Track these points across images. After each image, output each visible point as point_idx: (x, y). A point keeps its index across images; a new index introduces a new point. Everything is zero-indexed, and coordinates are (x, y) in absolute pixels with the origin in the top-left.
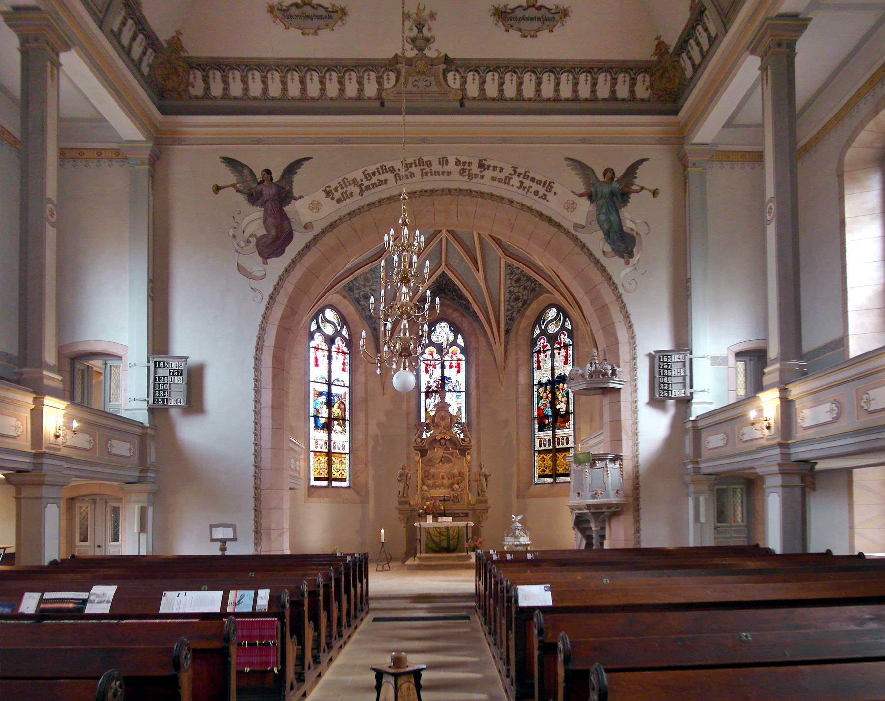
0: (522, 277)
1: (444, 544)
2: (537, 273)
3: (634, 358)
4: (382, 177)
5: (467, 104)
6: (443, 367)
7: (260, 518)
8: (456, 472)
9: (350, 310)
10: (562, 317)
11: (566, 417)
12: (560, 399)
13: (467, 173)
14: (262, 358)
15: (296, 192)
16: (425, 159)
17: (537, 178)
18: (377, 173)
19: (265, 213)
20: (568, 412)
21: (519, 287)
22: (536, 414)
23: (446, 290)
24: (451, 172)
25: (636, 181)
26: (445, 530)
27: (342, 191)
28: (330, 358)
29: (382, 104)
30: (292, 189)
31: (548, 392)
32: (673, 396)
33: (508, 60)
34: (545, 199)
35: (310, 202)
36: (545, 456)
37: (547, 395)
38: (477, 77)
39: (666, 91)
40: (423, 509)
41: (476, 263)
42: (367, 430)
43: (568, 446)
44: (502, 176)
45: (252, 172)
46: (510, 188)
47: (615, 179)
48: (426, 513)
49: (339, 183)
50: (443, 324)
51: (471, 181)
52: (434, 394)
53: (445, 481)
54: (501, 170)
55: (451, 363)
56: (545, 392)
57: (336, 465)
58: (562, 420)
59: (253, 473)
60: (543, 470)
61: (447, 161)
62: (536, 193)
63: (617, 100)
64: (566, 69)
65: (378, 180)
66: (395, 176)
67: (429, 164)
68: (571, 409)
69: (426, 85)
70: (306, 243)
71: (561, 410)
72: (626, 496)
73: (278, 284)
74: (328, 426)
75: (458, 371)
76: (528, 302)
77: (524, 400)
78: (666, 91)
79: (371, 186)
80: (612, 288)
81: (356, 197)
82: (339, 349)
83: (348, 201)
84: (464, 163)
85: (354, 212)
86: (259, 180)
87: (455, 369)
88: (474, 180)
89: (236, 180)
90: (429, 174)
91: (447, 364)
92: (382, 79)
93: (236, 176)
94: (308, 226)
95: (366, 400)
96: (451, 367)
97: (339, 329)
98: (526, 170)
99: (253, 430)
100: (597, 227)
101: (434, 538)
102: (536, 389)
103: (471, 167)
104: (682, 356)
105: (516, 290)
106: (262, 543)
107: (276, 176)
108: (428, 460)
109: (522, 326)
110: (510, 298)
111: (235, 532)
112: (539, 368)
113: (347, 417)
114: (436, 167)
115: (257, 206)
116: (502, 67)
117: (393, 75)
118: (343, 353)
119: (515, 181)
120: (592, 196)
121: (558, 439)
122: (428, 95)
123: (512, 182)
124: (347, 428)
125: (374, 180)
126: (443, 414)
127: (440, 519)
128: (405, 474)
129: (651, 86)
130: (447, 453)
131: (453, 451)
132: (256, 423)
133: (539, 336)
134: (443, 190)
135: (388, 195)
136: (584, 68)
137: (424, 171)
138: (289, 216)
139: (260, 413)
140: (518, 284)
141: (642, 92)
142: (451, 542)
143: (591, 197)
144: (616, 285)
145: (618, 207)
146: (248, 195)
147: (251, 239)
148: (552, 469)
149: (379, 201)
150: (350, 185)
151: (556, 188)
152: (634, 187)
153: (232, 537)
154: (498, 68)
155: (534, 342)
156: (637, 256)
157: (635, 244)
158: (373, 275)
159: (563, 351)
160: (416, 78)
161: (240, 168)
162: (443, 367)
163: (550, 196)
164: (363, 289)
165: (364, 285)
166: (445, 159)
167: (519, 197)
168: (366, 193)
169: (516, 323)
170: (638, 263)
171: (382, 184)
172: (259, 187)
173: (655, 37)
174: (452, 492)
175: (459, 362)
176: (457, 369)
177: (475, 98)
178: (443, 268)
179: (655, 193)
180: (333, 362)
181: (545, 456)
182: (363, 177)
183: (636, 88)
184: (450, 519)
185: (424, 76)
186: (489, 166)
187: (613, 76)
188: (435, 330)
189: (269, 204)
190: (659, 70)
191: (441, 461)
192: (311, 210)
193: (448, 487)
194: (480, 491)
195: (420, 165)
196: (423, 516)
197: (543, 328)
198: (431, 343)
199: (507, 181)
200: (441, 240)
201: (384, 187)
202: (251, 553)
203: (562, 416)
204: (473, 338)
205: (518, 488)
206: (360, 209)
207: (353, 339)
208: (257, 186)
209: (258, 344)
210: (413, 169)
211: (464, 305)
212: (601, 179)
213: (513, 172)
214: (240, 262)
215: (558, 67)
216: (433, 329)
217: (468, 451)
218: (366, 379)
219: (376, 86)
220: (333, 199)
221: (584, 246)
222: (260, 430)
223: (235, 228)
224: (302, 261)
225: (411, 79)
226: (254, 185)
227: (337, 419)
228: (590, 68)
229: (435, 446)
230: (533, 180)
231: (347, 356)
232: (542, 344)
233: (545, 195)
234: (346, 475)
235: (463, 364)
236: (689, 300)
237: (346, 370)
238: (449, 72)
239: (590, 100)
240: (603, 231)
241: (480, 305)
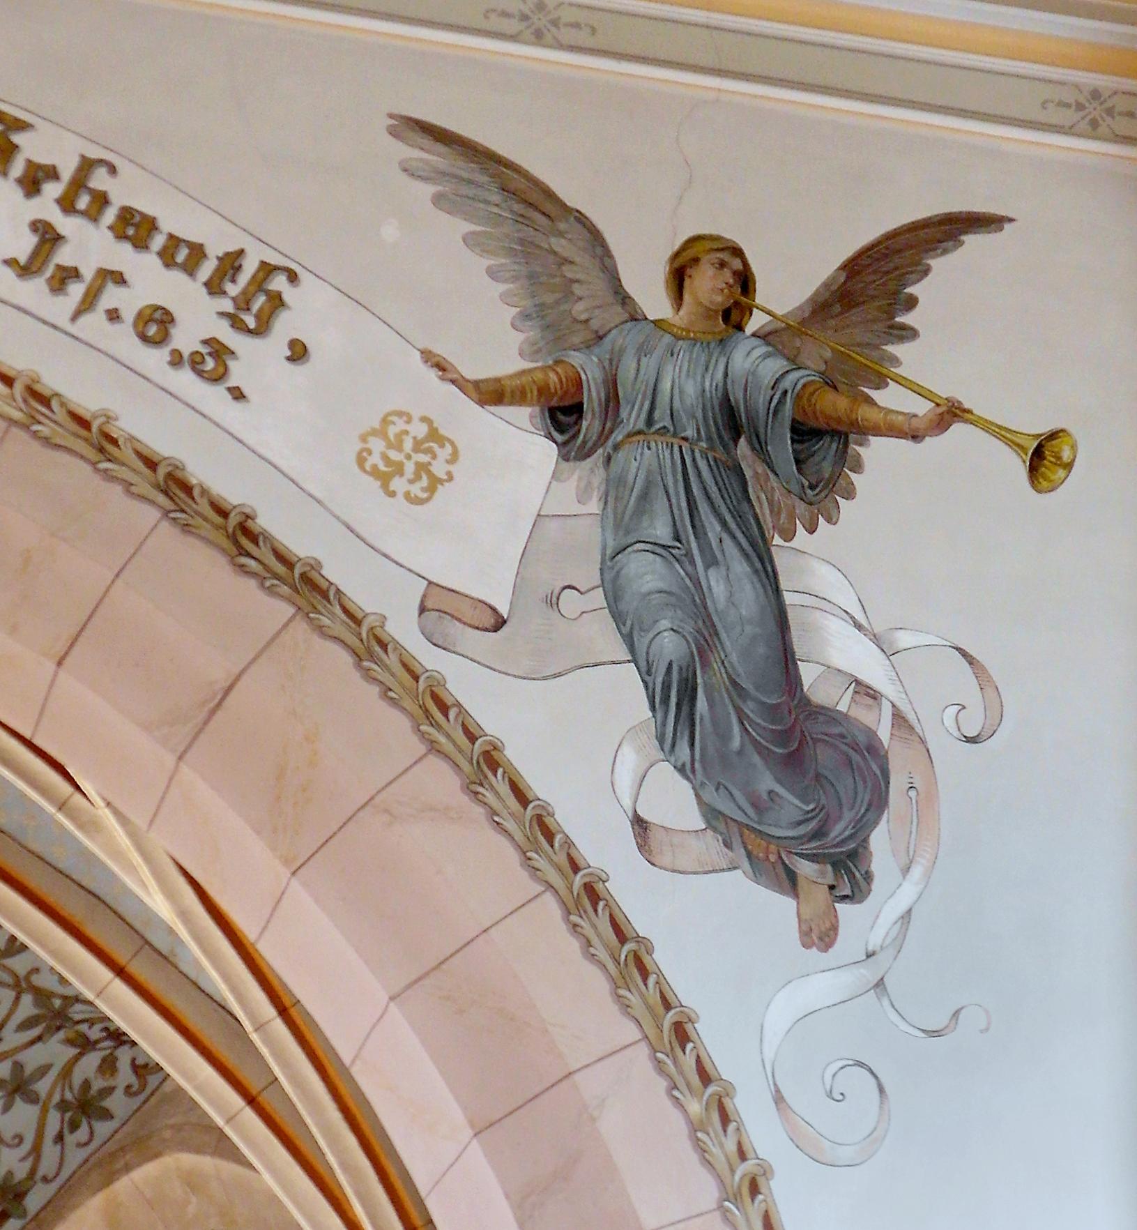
2: (120, 972)
17: (169, 223)
34: (217, 377)
47: (756, 322)
80: (695, 1108)
98: (94, 153)
120: (577, 410)
152: (890, 398)
157: (879, 802)
221: (492, 759)
240: (646, 673)
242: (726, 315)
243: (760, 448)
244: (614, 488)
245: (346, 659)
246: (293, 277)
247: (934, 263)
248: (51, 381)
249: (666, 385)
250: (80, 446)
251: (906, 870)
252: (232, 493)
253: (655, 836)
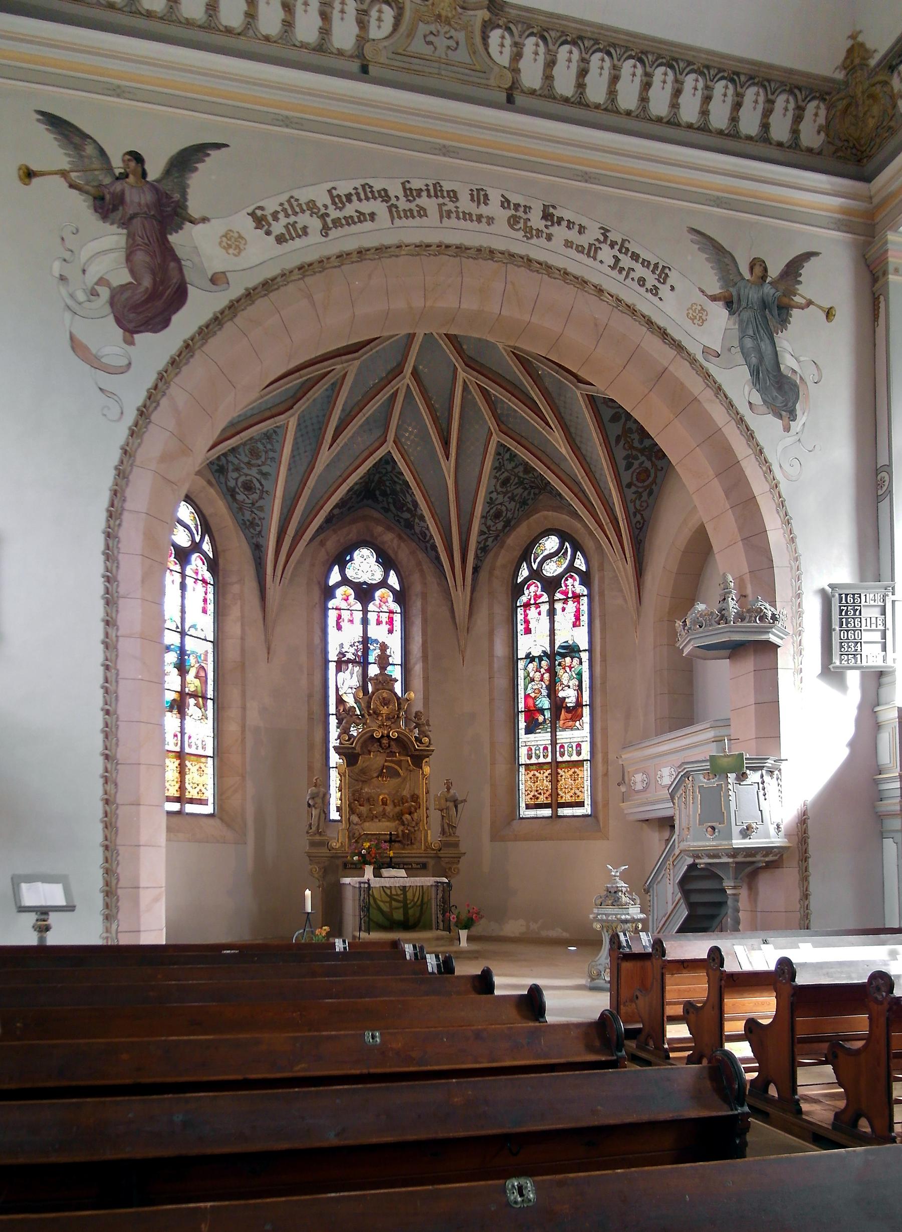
0: (513, 477)
1: (398, 915)
2: (548, 468)
3: (799, 596)
4: (367, 207)
5: (519, 99)
6: (365, 622)
7: (115, 864)
8: (406, 793)
9: (219, 508)
10: (569, 550)
11: (575, 712)
12: (565, 683)
13: (521, 225)
14: (122, 533)
15: (194, 207)
16: (446, 186)
17: (642, 256)
18: (354, 198)
19: (131, 241)
20: (579, 704)
21: (505, 494)
22: (521, 706)
23: (377, 493)
24: (493, 218)
25: (800, 288)
26: (399, 892)
27: (287, 220)
28: (183, 587)
29: (365, 69)
30: (186, 200)
31: (543, 671)
32: (864, 664)
33: (601, 27)
34: (656, 294)
35: (223, 232)
36: (537, 774)
37: (542, 675)
38: (542, 49)
39: (847, 141)
40: (359, 854)
41: (446, 443)
42: (244, 718)
43: (580, 758)
44: (584, 240)
45: (102, 152)
46: (596, 264)
47: (769, 280)
48: (365, 861)
49: (281, 204)
50: (365, 552)
51: (530, 241)
52: (350, 665)
53: (388, 809)
54: (582, 230)
55: (379, 617)
56: (538, 670)
57: (192, 776)
58: (570, 715)
59: (100, 770)
60: (534, 796)
61: (486, 196)
62: (642, 281)
63: (771, 144)
64: (695, 67)
65: (357, 211)
66: (390, 208)
67: (453, 196)
68: (586, 698)
69: (449, 47)
70: (215, 314)
71: (567, 700)
72: (788, 835)
73: (156, 387)
74: (179, 706)
75: (391, 631)
76: (512, 523)
77: (502, 682)
78: (847, 141)
79: (343, 222)
80: (764, 468)
81: (314, 237)
82: (197, 573)
83: (298, 243)
84: (517, 206)
85: (310, 265)
86: (117, 172)
87: (385, 627)
88: (534, 241)
89: (69, 163)
90: (454, 215)
91: (372, 617)
92: (367, 18)
93: (69, 155)
94: (218, 279)
95: (243, 666)
96: (379, 623)
97: (198, 539)
98: (625, 238)
99: (101, 680)
100: (740, 359)
101: (381, 904)
102: (521, 664)
103: (529, 216)
104: (878, 597)
105: (500, 499)
106: (120, 916)
107: (155, 170)
108: (361, 770)
109: (500, 561)
110: (489, 512)
111: (16, 893)
112: (528, 631)
113: (210, 694)
114: (465, 204)
115: (112, 224)
116: (590, 39)
117: (389, 13)
118: (204, 581)
119: (606, 254)
120: (732, 302)
121: (562, 747)
122: (450, 68)
123: (601, 255)
124: (210, 713)
125: (350, 210)
126: (385, 695)
127: (385, 872)
128: (321, 795)
129: (826, 128)
130: (392, 761)
131: (403, 758)
132: (107, 668)
133: (526, 580)
134: (479, 250)
135: (376, 244)
136: (724, 71)
137: (445, 208)
138: (180, 253)
139: (116, 648)
140: (504, 490)
141: (810, 137)
142: (411, 912)
143: (729, 304)
144: (771, 465)
145: (772, 328)
146: (95, 198)
147: (99, 289)
148: (551, 795)
149: (360, 252)
150: (303, 211)
151: (674, 277)
152: (797, 299)
153: (64, 904)
154: (581, 38)
155: (518, 590)
156: (801, 419)
157: (797, 398)
158: (269, 446)
159: (571, 606)
160: (432, 28)
161: (77, 140)
162: (365, 622)
163: (664, 290)
164: (246, 471)
165: (249, 464)
166: (482, 193)
167: (612, 283)
168: (333, 233)
169: (491, 554)
170: (803, 430)
171: (366, 220)
172: (118, 187)
173: (850, 34)
174: (401, 828)
175: (391, 615)
176: (388, 626)
177: (535, 90)
178: (389, 446)
179: (829, 314)
180: (188, 594)
181: (537, 774)
182: (328, 202)
183: (802, 126)
184: (402, 873)
185: (447, 28)
186: (560, 220)
187: (770, 97)
188: (352, 559)
189: (137, 222)
190: (842, 99)
191: (381, 774)
192: (224, 248)
193: (393, 819)
194: (446, 826)
195: (436, 196)
196: (357, 869)
197: (535, 567)
198: (345, 581)
199: (592, 251)
200: (395, 394)
201: (368, 225)
202: (99, 942)
203: (568, 710)
204: (416, 578)
205: (493, 823)
206: (322, 261)
207: (221, 561)
208: (112, 184)
209: (112, 505)
210: (424, 201)
211: (406, 520)
212: (747, 275)
213: (602, 238)
214: (74, 332)
215: (682, 60)
216: (348, 558)
217: (427, 759)
218: (243, 630)
219: (356, 30)
220: (268, 233)
221: (720, 388)
222: (117, 682)
223: (65, 260)
224: (204, 348)
225: (423, 28)
226: (107, 181)
227: (194, 695)
228: (735, 73)
229: (373, 749)
230: (635, 257)
231: (210, 589)
232: (532, 594)
233: (656, 288)
234: (209, 795)
235: (397, 618)
236: (884, 505)
237: (209, 612)
238: (491, 30)
239: (727, 135)
240: (749, 368)
241: (436, 518)
242: (762, 278)
243: (770, 312)
244: (741, 322)
245: (688, 364)
246: (670, 269)
247: (805, 264)
248: (622, 296)
249: (750, 296)
250: (628, 312)
251: (803, 414)
252: (662, 324)
253: (754, 407)
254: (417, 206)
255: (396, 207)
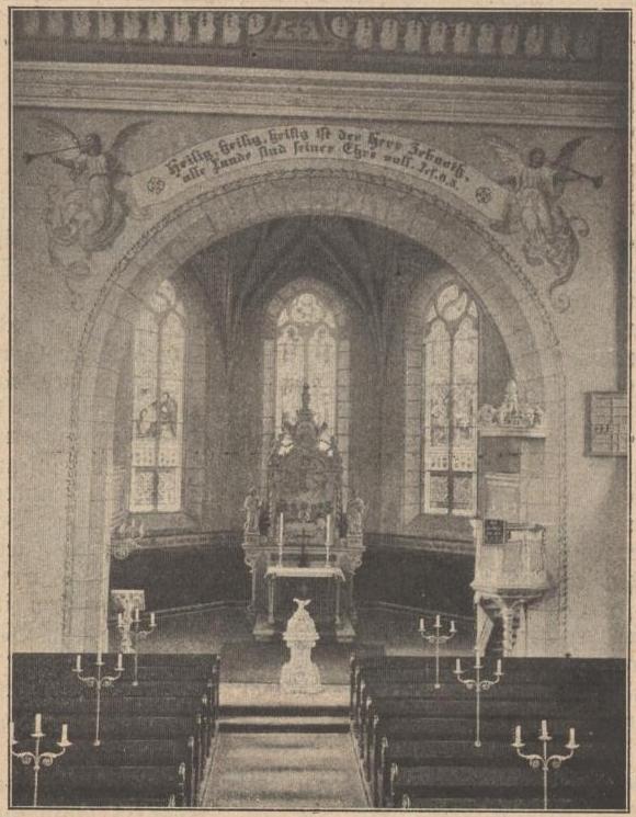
44: (399, 154)
84: (350, 136)
96: (318, 355)
125: (233, 154)
133: (434, 320)
150: (201, 159)
199: (406, 161)
213: (413, 151)
254: (280, 146)
255: (265, 148)
